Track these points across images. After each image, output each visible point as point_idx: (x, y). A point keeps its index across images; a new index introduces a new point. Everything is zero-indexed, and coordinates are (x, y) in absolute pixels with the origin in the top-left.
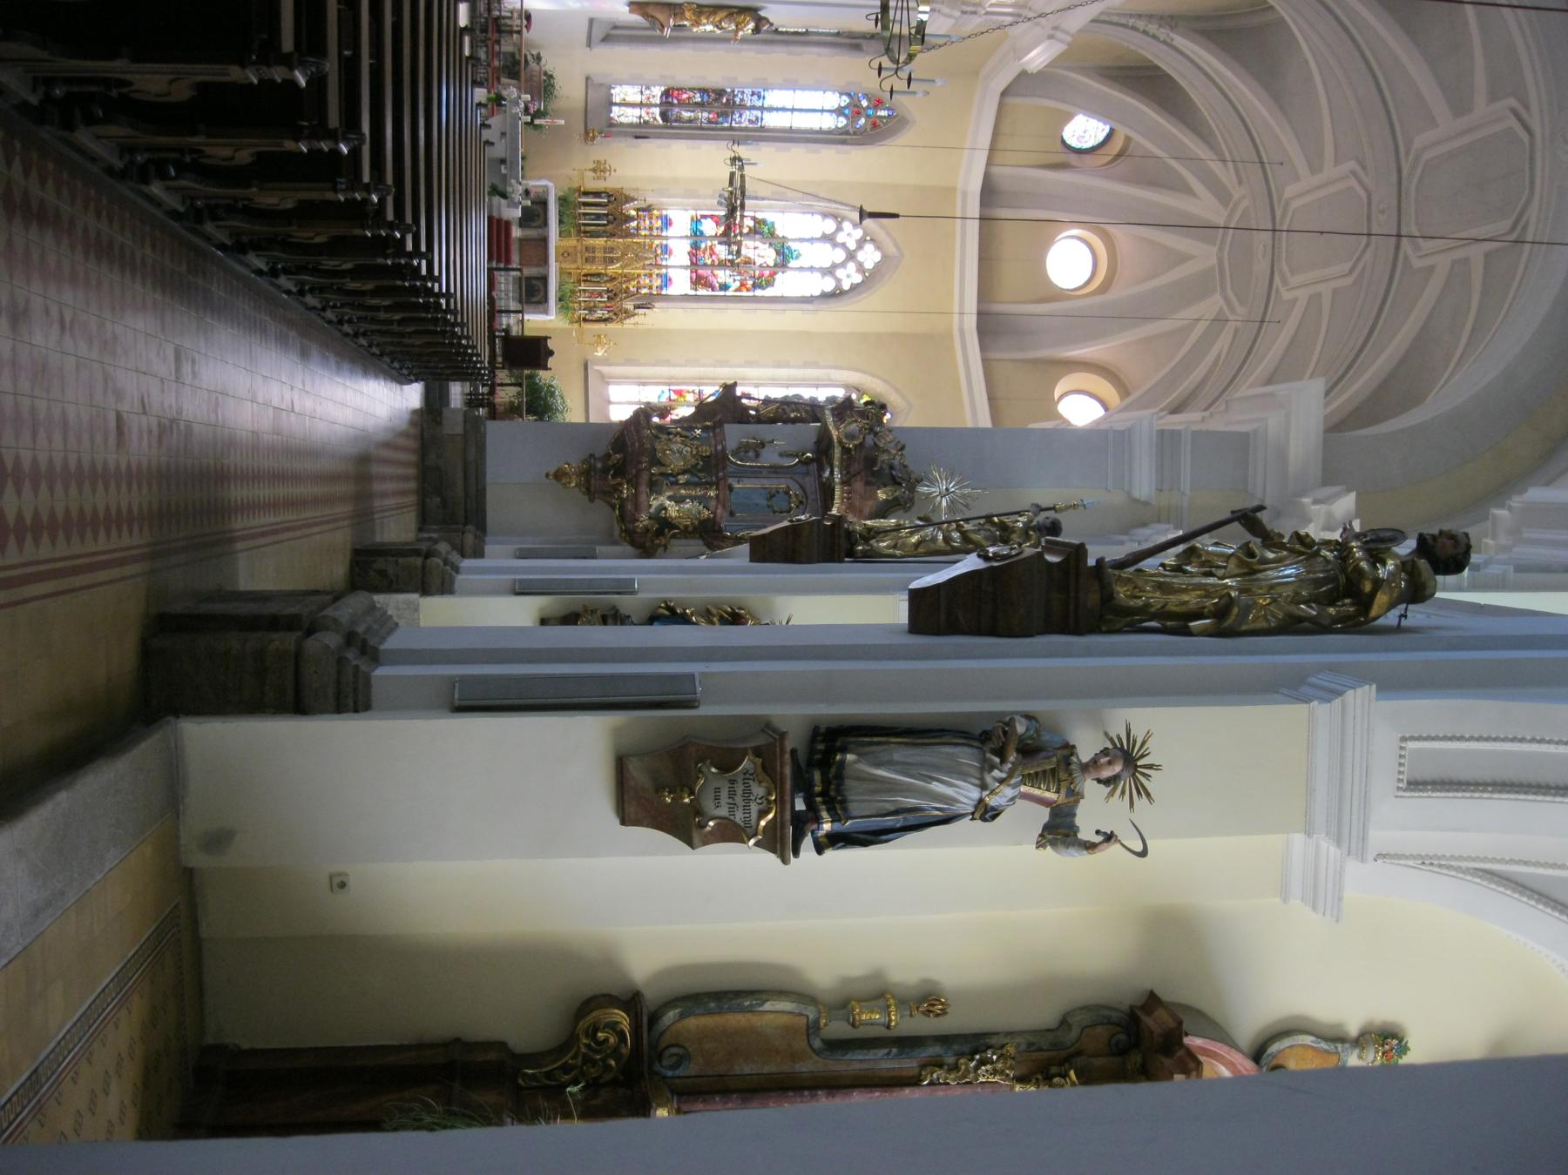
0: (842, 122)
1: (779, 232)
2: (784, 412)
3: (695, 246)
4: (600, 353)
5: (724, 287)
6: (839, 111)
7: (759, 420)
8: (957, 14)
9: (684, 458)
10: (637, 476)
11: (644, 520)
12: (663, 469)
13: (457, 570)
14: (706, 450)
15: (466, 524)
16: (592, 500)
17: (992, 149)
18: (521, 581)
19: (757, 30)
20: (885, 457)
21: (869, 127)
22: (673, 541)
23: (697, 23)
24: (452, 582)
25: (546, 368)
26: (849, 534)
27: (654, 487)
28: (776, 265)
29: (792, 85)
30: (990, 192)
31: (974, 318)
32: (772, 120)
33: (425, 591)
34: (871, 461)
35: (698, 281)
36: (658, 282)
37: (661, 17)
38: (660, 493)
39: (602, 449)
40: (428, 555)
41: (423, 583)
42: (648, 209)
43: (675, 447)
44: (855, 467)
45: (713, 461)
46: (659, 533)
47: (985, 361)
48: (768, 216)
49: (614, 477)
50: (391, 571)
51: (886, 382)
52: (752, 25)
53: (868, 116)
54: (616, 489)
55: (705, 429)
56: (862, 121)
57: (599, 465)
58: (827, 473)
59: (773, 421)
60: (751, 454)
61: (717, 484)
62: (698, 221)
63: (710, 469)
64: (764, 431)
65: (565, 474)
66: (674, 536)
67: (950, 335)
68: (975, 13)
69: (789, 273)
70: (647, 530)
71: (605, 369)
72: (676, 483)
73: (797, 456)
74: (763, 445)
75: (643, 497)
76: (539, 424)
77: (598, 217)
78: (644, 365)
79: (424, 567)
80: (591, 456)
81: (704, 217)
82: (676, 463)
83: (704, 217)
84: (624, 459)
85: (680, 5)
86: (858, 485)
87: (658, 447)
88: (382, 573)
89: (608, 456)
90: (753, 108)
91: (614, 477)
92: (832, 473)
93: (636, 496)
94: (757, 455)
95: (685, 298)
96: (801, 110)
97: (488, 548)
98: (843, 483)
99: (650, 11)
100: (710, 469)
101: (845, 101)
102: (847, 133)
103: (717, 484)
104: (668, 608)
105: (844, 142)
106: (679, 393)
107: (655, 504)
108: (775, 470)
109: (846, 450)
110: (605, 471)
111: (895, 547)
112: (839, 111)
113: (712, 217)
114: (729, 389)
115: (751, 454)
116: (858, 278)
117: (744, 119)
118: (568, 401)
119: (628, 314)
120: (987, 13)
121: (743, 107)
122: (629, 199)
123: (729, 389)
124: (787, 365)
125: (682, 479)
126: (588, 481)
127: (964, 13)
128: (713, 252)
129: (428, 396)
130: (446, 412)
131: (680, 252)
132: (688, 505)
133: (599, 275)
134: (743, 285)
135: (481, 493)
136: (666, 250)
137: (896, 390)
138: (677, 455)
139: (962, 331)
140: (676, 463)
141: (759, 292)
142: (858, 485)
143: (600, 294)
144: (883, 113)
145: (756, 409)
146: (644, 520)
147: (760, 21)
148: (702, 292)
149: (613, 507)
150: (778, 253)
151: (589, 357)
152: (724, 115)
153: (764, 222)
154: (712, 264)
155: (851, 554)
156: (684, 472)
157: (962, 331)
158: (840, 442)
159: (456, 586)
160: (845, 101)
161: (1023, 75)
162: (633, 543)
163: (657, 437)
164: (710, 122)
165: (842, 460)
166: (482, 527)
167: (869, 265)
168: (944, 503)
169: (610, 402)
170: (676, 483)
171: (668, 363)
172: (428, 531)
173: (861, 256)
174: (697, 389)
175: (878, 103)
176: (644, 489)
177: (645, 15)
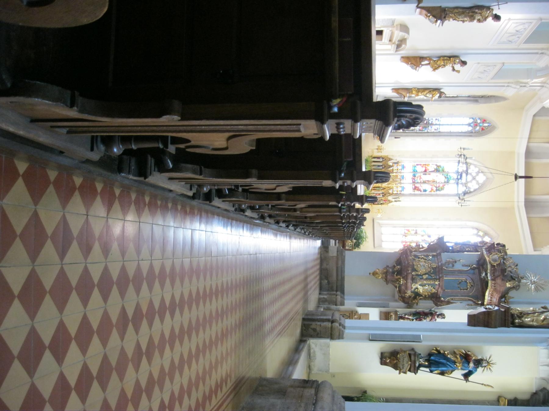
0: (470, 129)
1: (446, 170)
2: (461, 249)
3: (414, 176)
4: (379, 216)
5: (425, 191)
6: (469, 125)
7: (453, 251)
8: (518, 87)
10: (407, 276)
11: (409, 293)
13: (344, 327)
14: (434, 265)
15: (337, 291)
16: (387, 284)
17: (529, 138)
18: (372, 335)
19: (440, 97)
20: (510, 269)
21: (480, 130)
22: (420, 301)
23: (417, 95)
24: (343, 334)
26: (512, 315)
27: (414, 280)
28: (445, 182)
29: (451, 116)
30: (529, 153)
31: (523, 203)
32: (443, 129)
33: (332, 337)
34: (504, 271)
35: (416, 188)
36: (400, 189)
37: (404, 93)
38: (416, 283)
39: (391, 263)
40: (333, 322)
41: (331, 334)
42: (397, 163)
43: (422, 264)
44: (497, 274)
45: (437, 270)
46: (415, 298)
47: (528, 218)
48: (441, 164)
50: (318, 329)
52: (438, 95)
53: (480, 126)
54: (398, 280)
55: (433, 256)
56: (478, 128)
57: (391, 270)
58: (484, 275)
61: (439, 279)
62: (415, 166)
63: (437, 273)
64: (455, 256)
65: (377, 273)
66: (421, 299)
68: (525, 86)
69: (450, 185)
70: (410, 297)
71: (381, 222)
72: (422, 279)
73: (469, 266)
74: (456, 262)
75: (409, 284)
76: (494, 368)
77: (379, 166)
79: (332, 327)
80: (388, 266)
81: (418, 165)
82: (422, 270)
83: (418, 165)
84: (401, 268)
85: (411, 89)
86: (499, 281)
87: (414, 263)
88: (314, 330)
89: (394, 266)
90: (436, 124)
92: (486, 274)
93: (406, 284)
94: (453, 266)
95: (410, 195)
96: (448, 125)
97: (346, 302)
98: (492, 280)
99: (400, 91)
101: (471, 121)
102: (472, 133)
103: (439, 279)
104: (437, 350)
105: (471, 136)
107: (414, 287)
108: (460, 272)
109: (493, 266)
110: (393, 273)
111: (533, 321)
112: (469, 125)
113: (420, 165)
115: (451, 265)
116: (477, 187)
117: (432, 129)
118: (367, 234)
119: (390, 202)
120: (530, 86)
121: (432, 124)
122: (390, 159)
125: (425, 277)
126: (386, 276)
127: (521, 86)
128: (421, 178)
129: (323, 243)
130: (330, 248)
131: (408, 178)
132: (427, 287)
133: (379, 187)
134: (432, 190)
135: (343, 279)
136: (403, 177)
138: (422, 267)
139: (518, 206)
140: (422, 270)
141: (438, 192)
142: (499, 281)
143: (379, 194)
144: (486, 125)
145: (452, 247)
146: (409, 293)
147: (441, 93)
148: (417, 192)
149: (396, 287)
150: (446, 178)
152: (426, 128)
153: (440, 166)
154: (421, 183)
155: (514, 325)
156: (425, 274)
157: (518, 206)
158: (490, 263)
159: (345, 336)
160: (471, 121)
161: (543, 108)
162: (404, 301)
164: (420, 130)
165: (491, 270)
166: (343, 292)
167: (481, 181)
168: (533, 287)
169: (382, 234)
170: (422, 279)
172: (323, 294)
173: (477, 178)
174: (415, 229)
175: (484, 121)
176: (409, 281)
177: (398, 93)
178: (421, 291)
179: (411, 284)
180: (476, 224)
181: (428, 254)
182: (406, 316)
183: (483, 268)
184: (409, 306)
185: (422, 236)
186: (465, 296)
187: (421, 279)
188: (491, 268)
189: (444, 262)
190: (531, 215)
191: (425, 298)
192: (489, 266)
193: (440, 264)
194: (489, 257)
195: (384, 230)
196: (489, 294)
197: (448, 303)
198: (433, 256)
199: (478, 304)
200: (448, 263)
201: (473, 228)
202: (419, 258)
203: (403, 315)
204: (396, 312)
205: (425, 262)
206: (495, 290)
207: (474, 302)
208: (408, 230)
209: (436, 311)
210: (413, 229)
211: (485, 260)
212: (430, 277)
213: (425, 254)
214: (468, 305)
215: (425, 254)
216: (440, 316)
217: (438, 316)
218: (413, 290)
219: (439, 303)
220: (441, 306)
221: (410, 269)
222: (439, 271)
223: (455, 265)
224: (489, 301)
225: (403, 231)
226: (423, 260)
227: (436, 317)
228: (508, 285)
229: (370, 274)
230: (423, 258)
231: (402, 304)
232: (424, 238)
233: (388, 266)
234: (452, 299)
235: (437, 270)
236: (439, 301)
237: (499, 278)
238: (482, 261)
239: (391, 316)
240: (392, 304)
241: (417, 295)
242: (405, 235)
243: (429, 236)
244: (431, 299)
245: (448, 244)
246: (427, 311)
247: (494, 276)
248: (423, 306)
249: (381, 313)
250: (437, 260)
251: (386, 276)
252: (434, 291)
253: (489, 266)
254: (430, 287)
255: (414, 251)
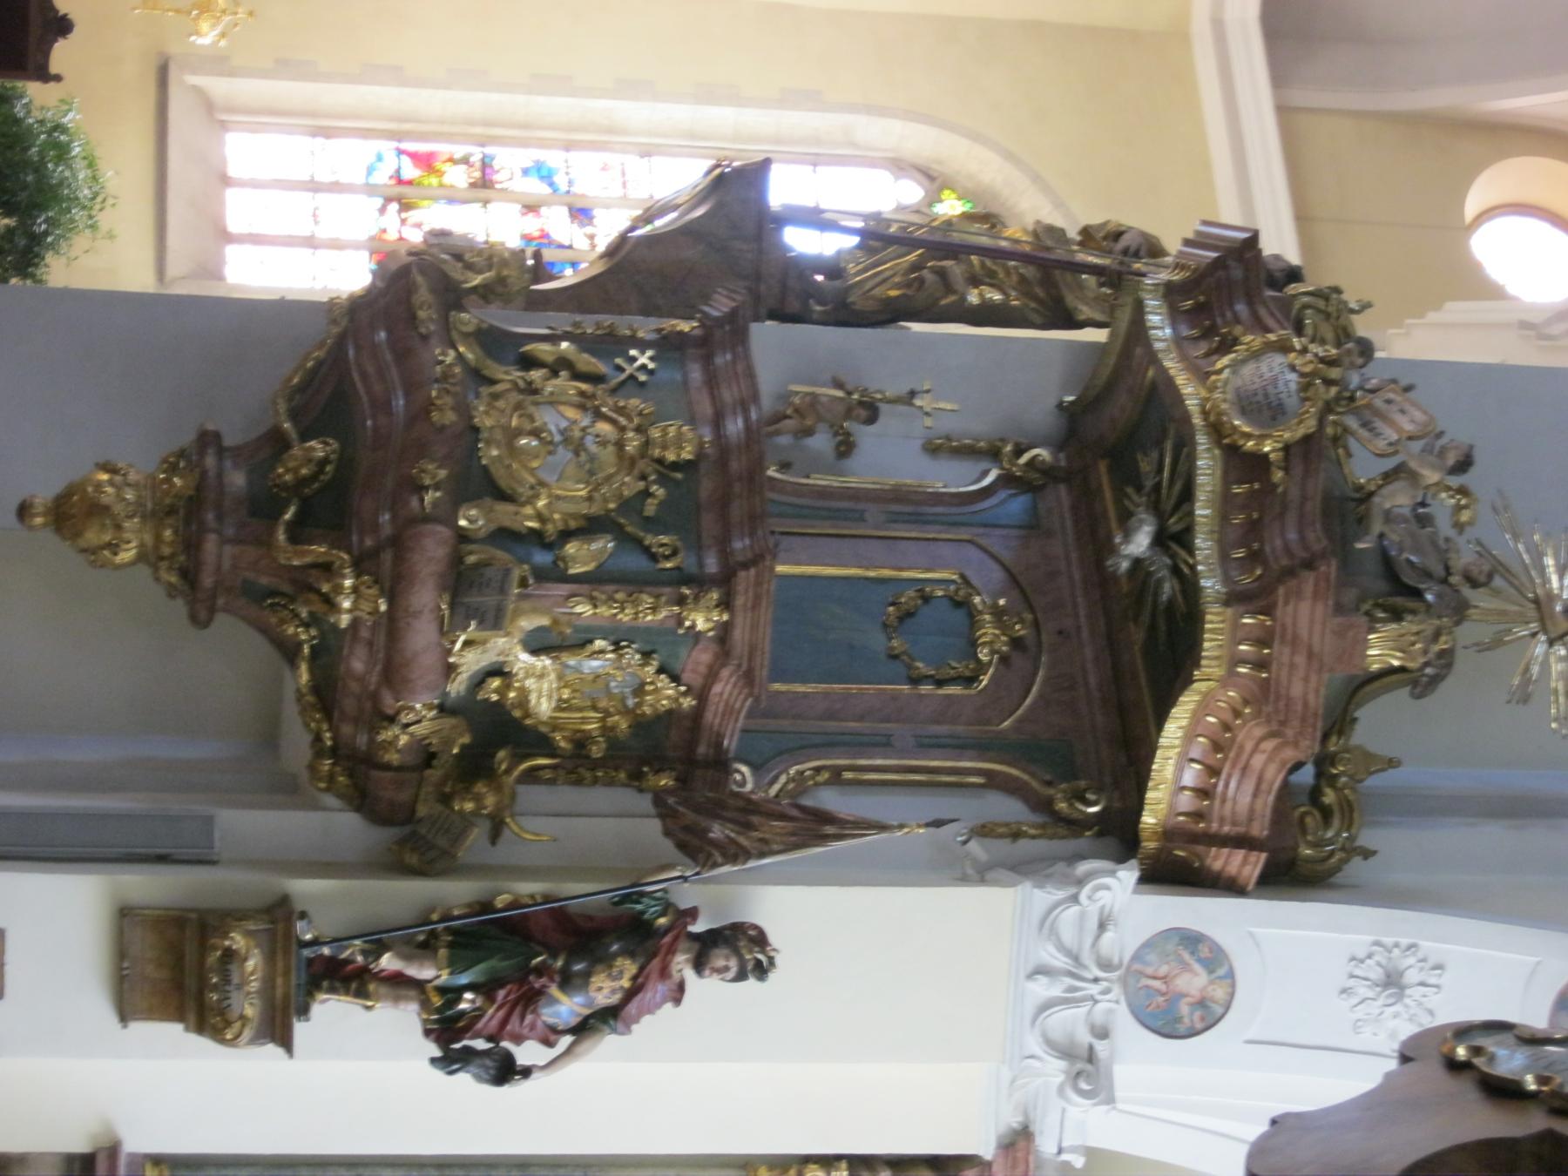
4: (207, 36)
7: (845, 313)
9: (590, 474)
10: (398, 543)
11: (418, 720)
12: (504, 514)
14: (681, 440)
16: (200, 620)
22: (531, 796)
25: (43, 74)
27: (470, 594)
38: (495, 620)
43: (552, 420)
44: (1284, 537)
45: (707, 487)
46: (475, 767)
47: (1284, 111)
49: (297, 534)
51: (1009, 156)
54: (308, 585)
55: (668, 346)
57: (237, 480)
59: (890, 314)
60: (821, 442)
63: (705, 516)
64: (869, 355)
65: (97, 510)
66: (531, 776)
67: (1180, 36)
70: (426, 756)
71: (218, 86)
73: (994, 454)
74: (870, 411)
75: (421, 636)
78: (328, 78)
80: (208, 439)
82: (555, 492)
84: (346, 463)
86: (1305, 613)
89: (277, 443)
91: (297, 534)
92: (1173, 540)
93: (393, 625)
94: (845, 447)
100: (705, 516)
103: (725, 580)
106: (425, 161)
107: (470, 662)
108: (909, 507)
109: (1243, 463)
110: (263, 506)
114: (736, 188)
115: (821, 442)
118: (108, 175)
123: (736, 188)
124: (734, 98)
125: (582, 555)
126: (191, 545)
132: (595, 663)
137: (1036, 179)
138: (560, 451)
139: (1218, 26)
140: (555, 492)
142: (1305, 613)
145: (834, 270)
146: (418, 720)
149: (289, 652)
151: (174, 49)
156: (590, 527)
157: (1218, 26)
158: (1217, 430)
162: (362, 800)
163: (479, 377)
165: (1226, 503)
169: (226, 181)
171: (396, 75)
174: (477, 154)
176: (426, 597)
178: (543, 707)
179: (446, 631)
180: (921, 141)
181: (625, 324)
182: (388, 962)
183: (1127, 476)
184: (417, 848)
185: (531, 208)
186: (960, 746)
187: (542, 576)
188: (1227, 481)
189: (767, 402)
190: (1300, 97)
191: (580, 762)
192: (1207, 467)
193: (735, 427)
194: (1203, 376)
195: (244, 151)
196: (1189, 736)
197: (816, 827)
198: (668, 346)
199: (1075, 826)
200: (806, 414)
201: (900, 166)
202: (528, 362)
203: (354, 952)
204: (279, 915)
205: (584, 403)
206: (1264, 696)
207: (1043, 805)
208: (425, 161)
209: (686, 896)
210: (459, 151)
211: (1161, 395)
212: (634, 562)
213: (590, 324)
214: (984, 831)
215: (590, 324)
216: (720, 958)
217: (706, 948)
218: (457, 687)
219: (717, 831)
220: (735, 854)
221: (435, 472)
222: (723, 503)
223: (866, 436)
224: (1186, 801)
225: (389, 162)
226: (563, 384)
227: (681, 964)
228: (1380, 650)
229: (24, 511)
230: (560, 366)
231: (343, 826)
232: (582, 187)
233: (208, 439)
234: (836, 777)
235: (707, 487)
236: (716, 810)
237: (1309, 580)
238: (1121, 408)
239: (229, 955)
240: (246, 824)
241: (494, 733)
242: (402, 196)
243: (581, 214)
244: (636, 778)
245: (801, 242)
246: (584, 892)
247: (1255, 557)
248: (559, 844)
249: (125, 915)
250: (712, 382)
251: (191, 545)
252: (665, 694)
253: (1207, 467)
254: (632, 657)
255: (486, 293)
